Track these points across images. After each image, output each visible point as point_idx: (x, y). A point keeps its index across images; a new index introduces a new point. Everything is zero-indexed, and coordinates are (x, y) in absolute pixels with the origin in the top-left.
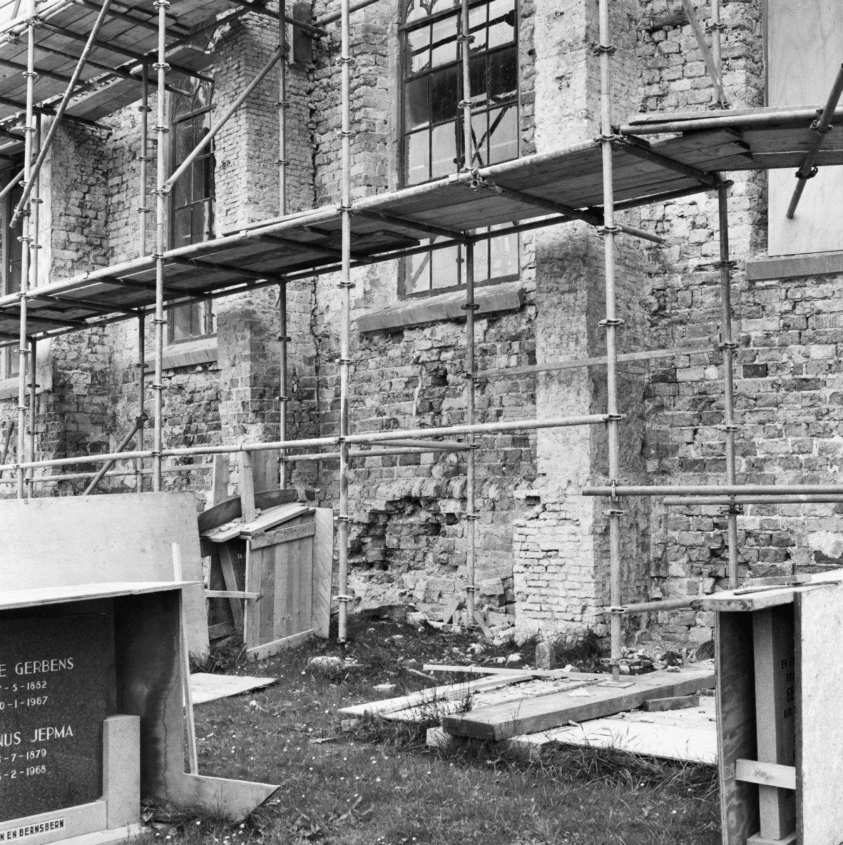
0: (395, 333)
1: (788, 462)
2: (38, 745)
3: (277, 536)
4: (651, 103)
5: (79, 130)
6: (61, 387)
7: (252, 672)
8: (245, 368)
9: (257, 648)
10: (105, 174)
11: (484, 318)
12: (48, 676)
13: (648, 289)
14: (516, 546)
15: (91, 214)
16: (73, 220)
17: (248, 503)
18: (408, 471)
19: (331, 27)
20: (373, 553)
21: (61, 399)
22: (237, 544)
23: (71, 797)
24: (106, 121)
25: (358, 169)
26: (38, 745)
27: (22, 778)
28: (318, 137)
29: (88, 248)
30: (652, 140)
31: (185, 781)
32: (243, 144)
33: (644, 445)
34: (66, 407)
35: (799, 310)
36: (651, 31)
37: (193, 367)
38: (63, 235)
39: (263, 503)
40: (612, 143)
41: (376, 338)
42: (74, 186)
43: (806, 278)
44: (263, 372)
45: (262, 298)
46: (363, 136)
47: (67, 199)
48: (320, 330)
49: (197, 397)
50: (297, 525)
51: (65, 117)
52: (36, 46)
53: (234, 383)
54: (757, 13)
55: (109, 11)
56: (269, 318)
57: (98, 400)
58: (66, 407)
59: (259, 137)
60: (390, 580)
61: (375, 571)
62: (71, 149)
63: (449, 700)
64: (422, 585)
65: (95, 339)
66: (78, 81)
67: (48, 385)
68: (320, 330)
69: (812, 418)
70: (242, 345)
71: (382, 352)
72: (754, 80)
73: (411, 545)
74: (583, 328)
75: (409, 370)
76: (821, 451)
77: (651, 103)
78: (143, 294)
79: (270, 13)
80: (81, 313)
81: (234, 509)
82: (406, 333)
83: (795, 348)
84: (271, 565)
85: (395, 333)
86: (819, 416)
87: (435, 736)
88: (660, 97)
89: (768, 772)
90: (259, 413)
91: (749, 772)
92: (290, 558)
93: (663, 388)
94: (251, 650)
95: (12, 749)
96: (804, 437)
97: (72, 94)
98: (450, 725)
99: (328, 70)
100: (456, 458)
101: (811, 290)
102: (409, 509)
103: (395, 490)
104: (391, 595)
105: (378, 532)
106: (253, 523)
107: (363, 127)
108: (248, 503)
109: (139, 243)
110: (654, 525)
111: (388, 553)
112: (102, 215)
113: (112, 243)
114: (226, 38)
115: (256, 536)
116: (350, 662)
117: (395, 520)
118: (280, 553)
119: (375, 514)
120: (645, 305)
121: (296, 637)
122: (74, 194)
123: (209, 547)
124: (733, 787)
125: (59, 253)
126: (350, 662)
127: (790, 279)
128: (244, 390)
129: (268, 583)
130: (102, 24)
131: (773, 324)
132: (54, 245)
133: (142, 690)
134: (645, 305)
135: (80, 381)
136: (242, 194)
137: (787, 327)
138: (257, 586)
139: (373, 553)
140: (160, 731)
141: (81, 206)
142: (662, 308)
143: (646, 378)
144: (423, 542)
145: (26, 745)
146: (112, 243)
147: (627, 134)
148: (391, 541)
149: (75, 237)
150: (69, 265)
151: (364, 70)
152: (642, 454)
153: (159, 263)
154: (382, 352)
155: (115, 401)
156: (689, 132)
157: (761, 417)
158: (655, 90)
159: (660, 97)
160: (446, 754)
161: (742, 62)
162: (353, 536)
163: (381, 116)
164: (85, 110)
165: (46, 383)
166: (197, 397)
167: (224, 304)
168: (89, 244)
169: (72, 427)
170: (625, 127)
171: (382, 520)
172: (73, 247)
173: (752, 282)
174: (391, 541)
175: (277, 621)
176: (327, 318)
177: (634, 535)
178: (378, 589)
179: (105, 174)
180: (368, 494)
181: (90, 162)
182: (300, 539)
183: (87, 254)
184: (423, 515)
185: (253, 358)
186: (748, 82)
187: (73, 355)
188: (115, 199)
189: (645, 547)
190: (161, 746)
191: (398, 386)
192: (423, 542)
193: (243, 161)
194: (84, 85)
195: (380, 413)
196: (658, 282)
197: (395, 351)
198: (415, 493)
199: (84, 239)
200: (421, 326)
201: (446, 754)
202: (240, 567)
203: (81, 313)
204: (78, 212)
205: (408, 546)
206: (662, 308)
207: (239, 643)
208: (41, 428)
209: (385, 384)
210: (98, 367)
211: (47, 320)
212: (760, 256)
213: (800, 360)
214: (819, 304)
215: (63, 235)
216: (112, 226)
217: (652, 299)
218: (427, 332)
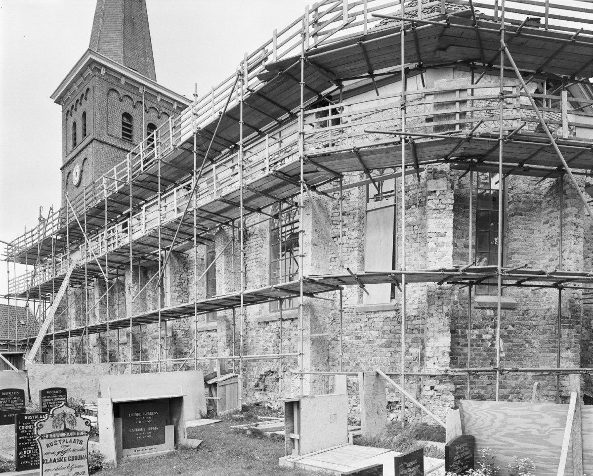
0: (267, 323)
1: (366, 363)
2: (149, 431)
3: (226, 382)
4: (333, 260)
5: (179, 255)
6: (174, 335)
7: (217, 419)
8: (224, 333)
9: (220, 412)
10: (187, 269)
11: (386, 281)
12: (152, 416)
13: (331, 314)
14: (291, 386)
15: (183, 281)
16: (177, 283)
17: (219, 374)
18: (270, 363)
19: (250, 228)
20: (262, 387)
21: (175, 339)
22: (215, 384)
23: (157, 443)
24: (187, 252)
25: (257, 273)
26: (149, 431)
27: (146, 438)
28: (247, 262)
29: (182, 292)
30: (316, 279)
31: (184, 441)
32: (223, 265)
33: (328, 358)
34: (176, 342)
35: (370, 321)
36: (333, 238)
37: (213, 330)
38: (174, 288)
39: (223, 373)
40: (303, 281)
41: (262, 324)
42: (177, 273)
43: (371, 312)
44: (230, 334)
45: (229, 312)
46: (259, 263)
47: (175, 277)
48: (247, 321)
49: (214, 339)
50: (233, 379)
51: (173, 252)
52: (161, 233)
53: (221, 337)
54: (362, 233)
55: (182, 224)
56: (230, 318)
57: (186, 339)
58: (176, 342)
59: (228, 263)
60: (266, 394)
61: (262, 392)
62: (176, 261)
63: (252, 425)
64: (273, 396)
65: (185, 320)
66: (176, 242)
67: (171, 335)
68: (247, 321)
69: (372, 351)
70: (224, 326)
71: (264, 328)
72: (361, 253)
73: (271, 385)
74: (309, 326)
75: (271, 334)
76: (374, 360)
77: (333, 260)
78: (192, 311)
79: (230, 225)
80: (178, 314)
81: (215, 375)
82: (270, 323)
83: (368, 332)
84: (225, 390)
85: (267, 323)
86: (374, 351)
87: (249, 432)
88: (335, 258)
89: (295, 436)
90: (229, 346)
91: (292, 436)
92: (231, 389)
93: (334, 342)
94: (219, 413)
95: (143, 431)
96: (370, 357)
97: (174, 245)
98: (251, 430)
99: (249, 242)
100: (283, 360)
101: (373, 315)
102: (271, 374)
103: (267, 369)
104: (265, 399)
105: (263, 380)
106: (219, 379)
107: (259, 260)
108: (219, 374)
109: (197, 294)
110: (330, 380)
111: (265, 386)
112: (186, 282)
113: (190, 290)
114: (219, 232)
115: (220, 382)
116: (242, 416)
117: (267, 377)
118: (228, 387)
119: (262, 375)
120: (329, 318)
121: (233, 409)
122: (177, 275)
123: (207, 385)
124: (289, 439)
125: (173, 294)
126: (242, 416)
127: (367, 312)
128: (224, 339)
129: (224, 395)
130: (180, 228)
131: (363, 325)
132: (171, 291)
133: (175, 420)
134: (329, 318)
135: (180, 334)
136: (223, 281)
137: (366, 325)
138: (221, 396)
139: (262, 387)
140: (179, 429)
141: (180, 279)
142: (334, 319)
143: (330, 339)
144: (274, 384)
145: (146, 431)
146: (190, 290)
147: (308, 279)
148: (266, 383)
149: (178, 289)
150: (176, 297)
151: (259, 242)
152: (328, 360)
153: (196, 305)
154: (264, 328)
155: (191, 339)
156: (325, 278)
157: (359, 351)
158: (334, 256)
159: (335, 258)
160: (250, 436)
161: (357, 248)
162: (256, 382)
163: (264, 257)
164: (325, 62)
165: (170, 334)
166: (214, 339)
167: (220, 313)
168: (183, 291)
169: (178, 347)
170: (307, 277)
171: (264, 377)
172: (177, 292)
173: (357, 313)
174: (266, 383)
175: (227, 405)
176: (249, 317)
177: (323, 383)
178: (262, 397)
179: (187, 269)
180: (260, 369)
181: (182, 265)
182: (225, 385)
183: (182, 294)
184: (274, 376)
185: (227, 330)
186: (358, 255)
187: (178, 325)
188: (190, 277)
189: (327, 386)
190: (179, 432)
191: (268, 339)
192: (274, 384)
193: (223, 271)
194: (177, 243)
195: (263, 346)
196: (333, 312)
197: (267, 328)
198: (272, 370)
199: (181, 289)
200: (274, 321)
201: (250, 436)
202: (216, 390)
203: (178, 314)
204: (179, 281)
205: (270, 385)
206: (334, 319)
207: (215, 410)
208: (169, 348)
209: (265, 338)
210: (186, 329)
211: (169, 316)
212: (360, 305)
213: (369, 335)
214: (375, 320)
215: (174, 288)
216: (189, 285)
217: (332, 317)
218: (275, 323)
